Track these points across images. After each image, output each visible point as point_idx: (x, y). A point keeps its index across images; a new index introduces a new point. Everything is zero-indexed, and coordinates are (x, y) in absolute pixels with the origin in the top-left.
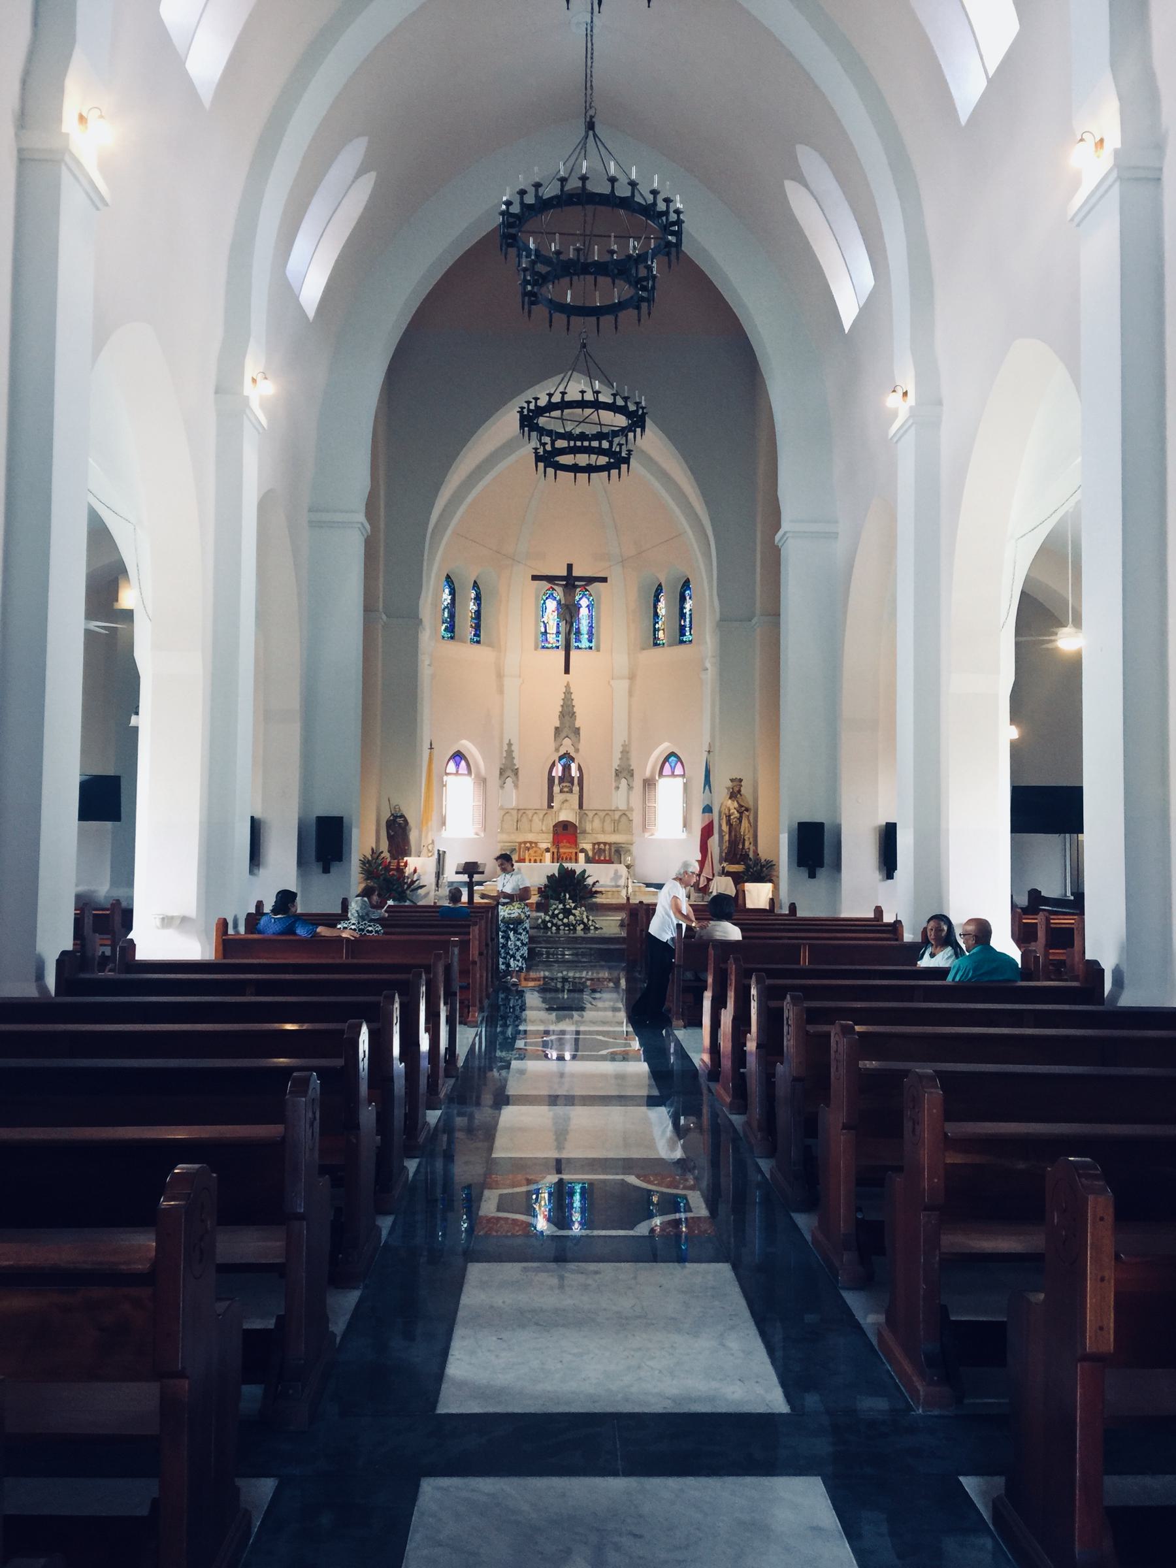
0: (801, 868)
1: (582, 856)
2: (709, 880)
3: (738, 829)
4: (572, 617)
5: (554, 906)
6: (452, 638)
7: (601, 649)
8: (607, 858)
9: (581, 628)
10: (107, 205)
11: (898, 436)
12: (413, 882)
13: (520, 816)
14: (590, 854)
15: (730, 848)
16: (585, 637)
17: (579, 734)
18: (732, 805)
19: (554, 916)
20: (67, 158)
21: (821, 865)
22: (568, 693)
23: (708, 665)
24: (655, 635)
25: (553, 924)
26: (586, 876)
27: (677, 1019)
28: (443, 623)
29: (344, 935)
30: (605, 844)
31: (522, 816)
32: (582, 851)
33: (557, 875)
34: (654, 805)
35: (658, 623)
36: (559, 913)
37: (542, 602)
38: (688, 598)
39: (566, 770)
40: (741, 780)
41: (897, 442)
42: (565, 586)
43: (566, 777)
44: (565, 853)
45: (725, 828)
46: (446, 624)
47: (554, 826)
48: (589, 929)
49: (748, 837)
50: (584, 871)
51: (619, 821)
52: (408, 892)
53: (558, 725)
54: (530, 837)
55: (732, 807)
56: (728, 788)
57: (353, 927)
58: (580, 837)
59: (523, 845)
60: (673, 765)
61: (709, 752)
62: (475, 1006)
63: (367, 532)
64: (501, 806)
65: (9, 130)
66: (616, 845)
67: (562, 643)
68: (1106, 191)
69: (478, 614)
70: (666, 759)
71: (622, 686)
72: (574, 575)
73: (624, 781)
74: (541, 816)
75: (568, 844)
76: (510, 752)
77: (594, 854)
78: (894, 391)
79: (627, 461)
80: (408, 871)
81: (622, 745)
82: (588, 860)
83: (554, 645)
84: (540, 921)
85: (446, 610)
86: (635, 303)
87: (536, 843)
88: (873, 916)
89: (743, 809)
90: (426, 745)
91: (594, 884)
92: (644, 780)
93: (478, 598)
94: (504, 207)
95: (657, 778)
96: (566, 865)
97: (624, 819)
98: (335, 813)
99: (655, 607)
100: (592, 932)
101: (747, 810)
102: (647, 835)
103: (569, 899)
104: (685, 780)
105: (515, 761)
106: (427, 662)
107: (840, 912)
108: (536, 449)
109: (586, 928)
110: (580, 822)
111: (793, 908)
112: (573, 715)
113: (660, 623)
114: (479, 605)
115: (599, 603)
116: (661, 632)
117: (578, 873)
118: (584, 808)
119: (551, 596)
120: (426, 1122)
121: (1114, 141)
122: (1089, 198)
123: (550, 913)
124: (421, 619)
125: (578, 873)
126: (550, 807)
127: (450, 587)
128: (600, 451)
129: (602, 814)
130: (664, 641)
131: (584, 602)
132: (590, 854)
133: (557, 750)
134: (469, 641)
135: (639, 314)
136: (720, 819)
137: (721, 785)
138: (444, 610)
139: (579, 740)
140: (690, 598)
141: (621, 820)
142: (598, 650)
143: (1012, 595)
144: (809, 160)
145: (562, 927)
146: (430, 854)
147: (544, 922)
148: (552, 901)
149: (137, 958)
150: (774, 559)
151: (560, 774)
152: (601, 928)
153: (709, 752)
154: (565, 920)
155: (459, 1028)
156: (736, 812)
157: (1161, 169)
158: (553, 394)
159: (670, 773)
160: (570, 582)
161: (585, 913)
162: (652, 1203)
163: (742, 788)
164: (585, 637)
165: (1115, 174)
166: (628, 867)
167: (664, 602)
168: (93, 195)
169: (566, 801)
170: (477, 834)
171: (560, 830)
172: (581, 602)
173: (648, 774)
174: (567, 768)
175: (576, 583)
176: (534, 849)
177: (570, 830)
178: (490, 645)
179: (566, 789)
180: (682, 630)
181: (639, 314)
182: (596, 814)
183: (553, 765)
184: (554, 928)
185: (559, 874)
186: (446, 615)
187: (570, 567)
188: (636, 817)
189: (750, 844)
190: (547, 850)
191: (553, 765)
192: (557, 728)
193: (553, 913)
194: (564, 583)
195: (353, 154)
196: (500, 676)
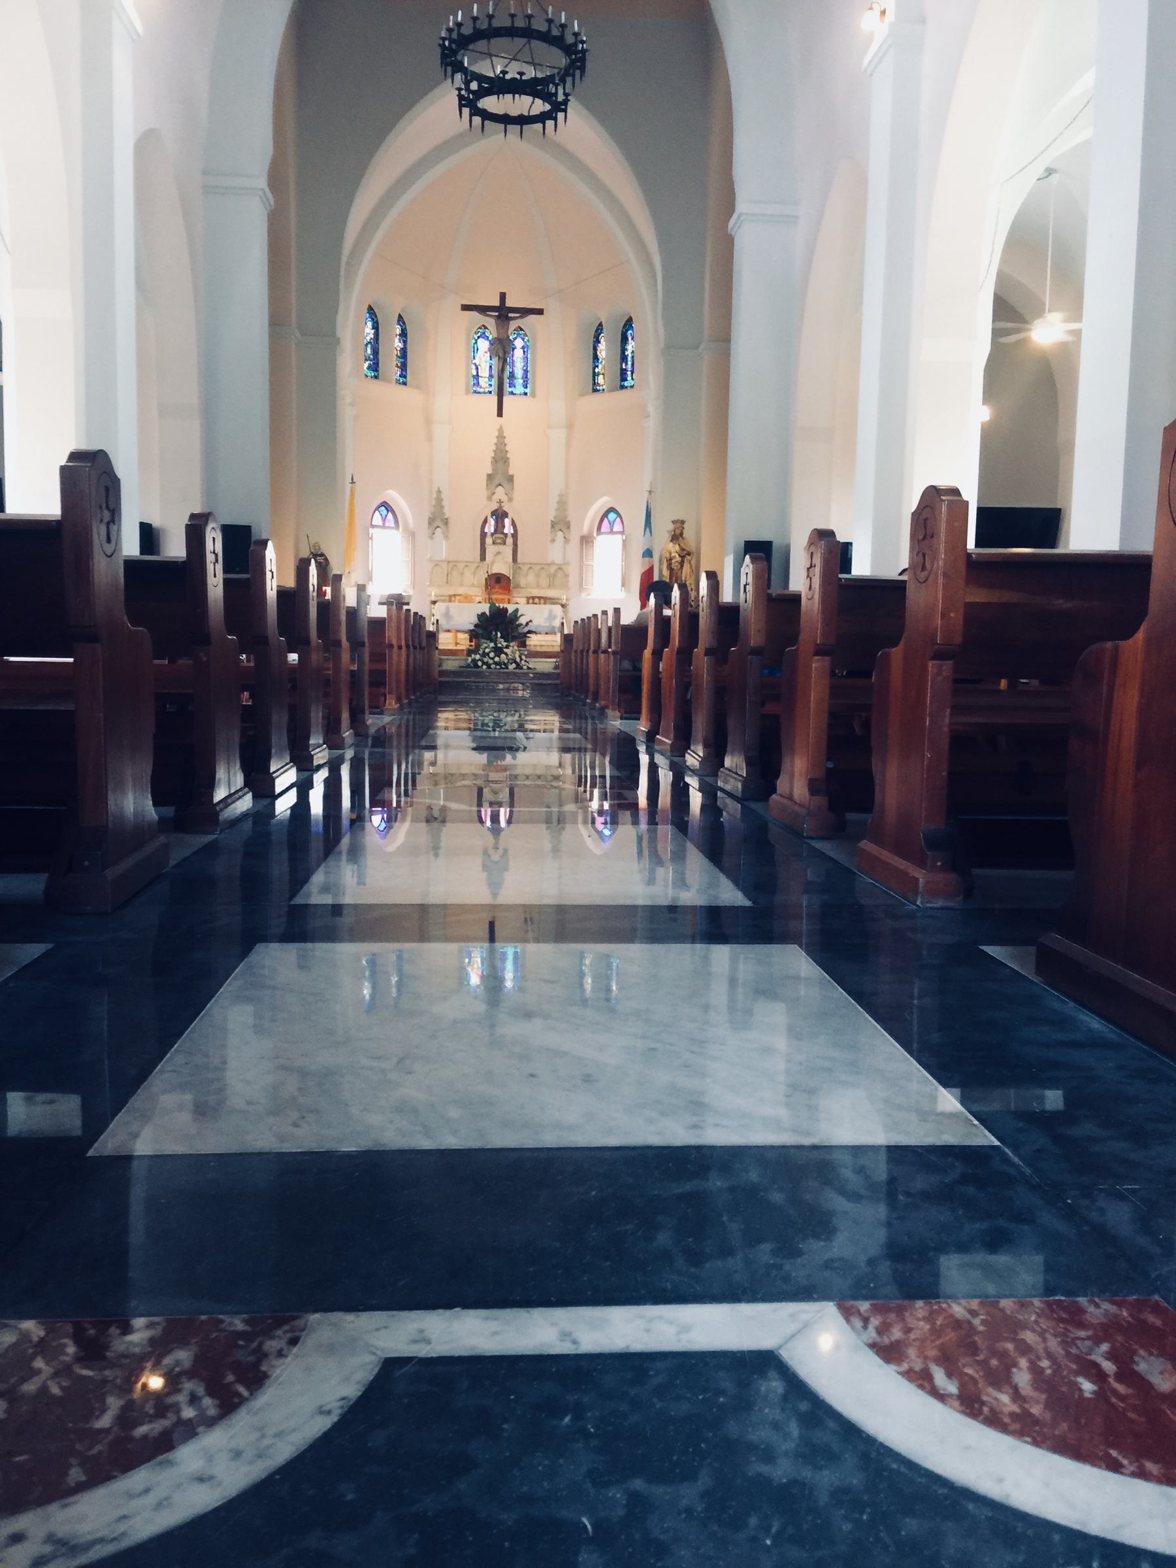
3: (679, 574)
4: (505, 353)
5: (485, 645)
6: (376, 377)
9: (516, 371)
13: (450, 569)
16: (519, 382)
17: (513, 482)
18: (674, 548)
19: (485, 655)
22: (501, 437)
23: (651, 409)
24: (594, 380)
25: (483, 663)
26: (519, 615)
27: (613, 709)
28: (366, 360)
31: (452, 569)
33: (488, 614)
35: (597, 366)
36: (490, 652)
37: (474, 341)
38: (630, 338)
40: (683, 522)
42: (498, 317)
46: (369, 362)
51: (554, 576)
53: (490, 472)
61: (650, 492)
62: (392, 694)
63: (270, 205)
67: (494, 388)
69: (404, 352)
70: (605, 515)
72: (507, 305)
74: (473, 570)
75: (500, 591)
76: (439, 500)
78: (871, 9)
81: (559, 495)
83: (487, 390)
85: (369, 346)
86: (542, 118)
93: (404, 334)
95: (595, 535)
97: (560, 574)
99: (595, 349)
101: (689, 554)
102: (583, 595)
103: (501, 637)
104: (624, 537)
106: (348, 400)
112: (506, 461)
113: (600, 366)
114: (405, 342)
116: (601, 377)
117: (510, 611)
118: (519, 561)
123: (481, 652)
124: (339, 339)
125: (510, 611)
126: (483, 557)
127: (373, 319)
130: (604, 387)
131: (519, 343)
134: (394, 382)
136: (660, 561)
137: (663, 528)
138: (367, 345)
139: (513, 489)
140: (632, 339)
142: (534, 395)
143: (993, 249)
145: (493, 666)
148: (483, 641)
150: (727, 245)
153: (650, 492)
154: (497, 659)
156: (677, 556)
159: (609, 530)
160: (503, 313)
162: (585, 965)
163: (684, 531)
164: (519, 382)
166: (563, 606)
167: (604, 343)
169: (499, 553)
173: (585, 531)
175: (510, 315)
177: (503, 583)
178: (418, 387)
179: (499, 541)
180: (623, 373)
182: (531, 568)
183: (485, 521)
186: (369, 351)
187: (503, 296)
188: (573, 571)
191: (485, 521)
192: (489, 476)
193: (484, 652)
194: (497, 314)
196: (428, 422)
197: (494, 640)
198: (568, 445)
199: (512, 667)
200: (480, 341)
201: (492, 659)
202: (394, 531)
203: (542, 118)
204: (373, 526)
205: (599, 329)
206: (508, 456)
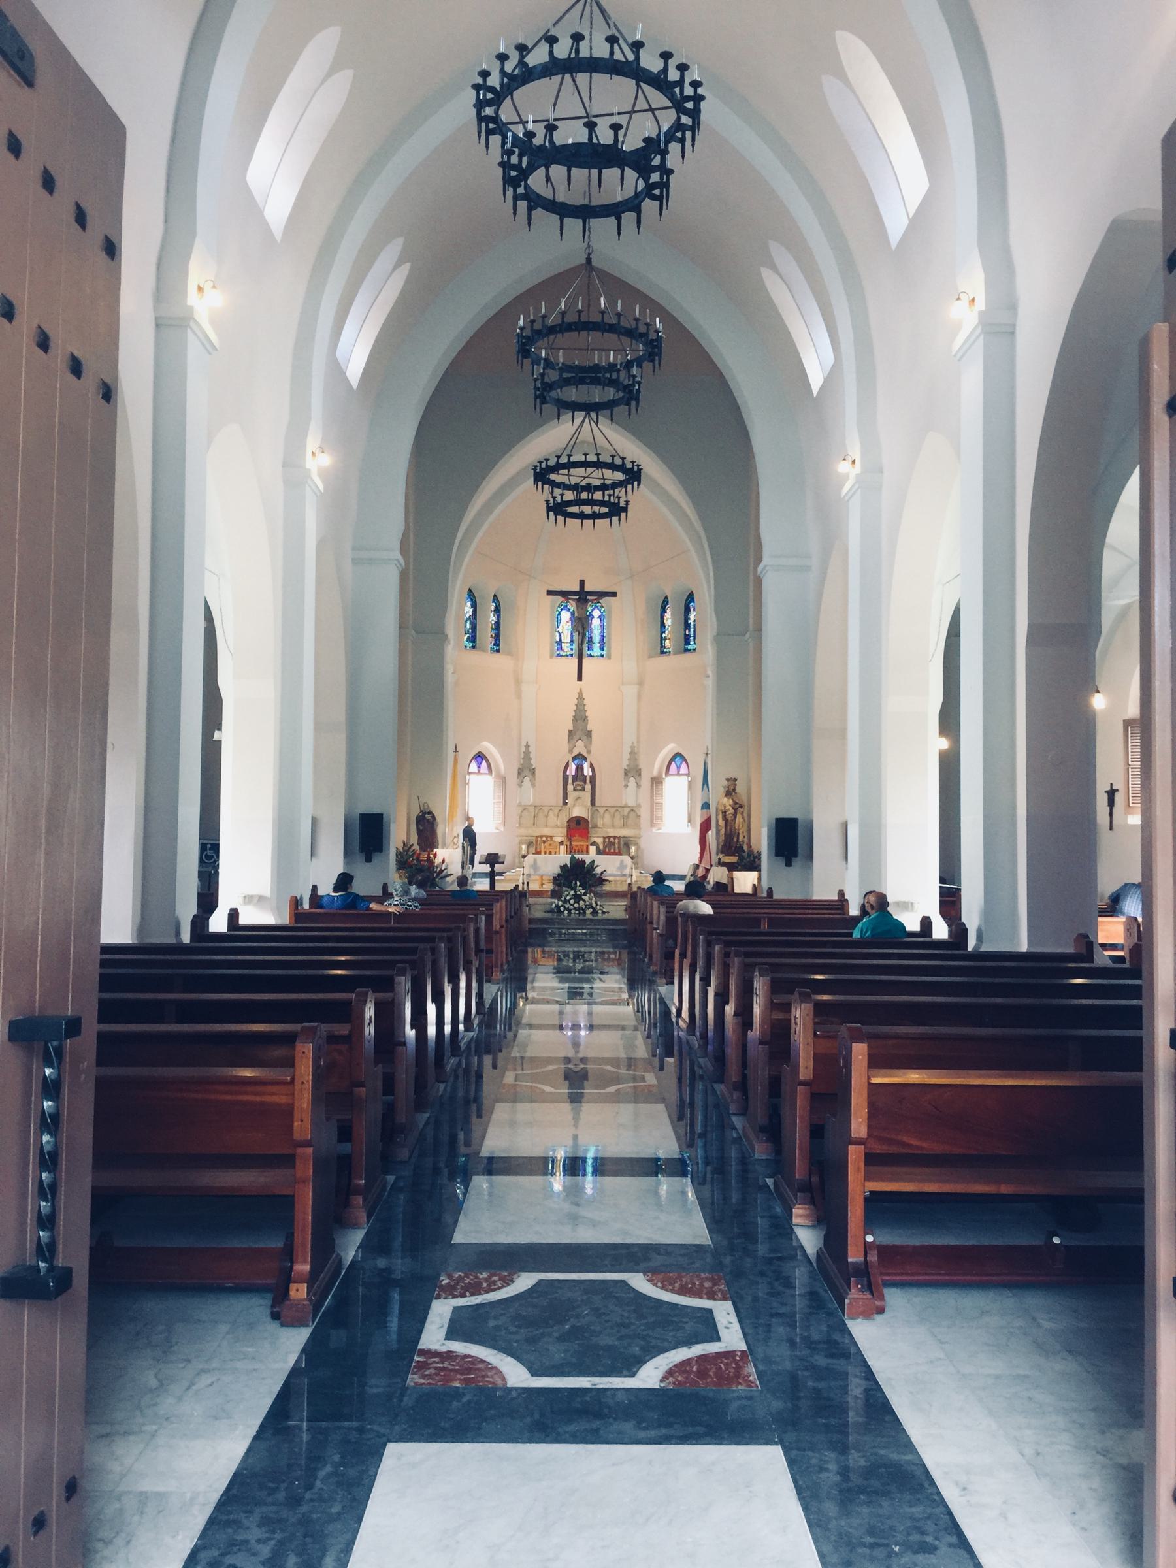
0: (779, 858)
1: (593, 849)
2: (707, 870)
5: (566, 893)
6: (474, 647)
7: (612, 657)
8: (617, 851)
10: (216, 350)
11: (850, 494)
12: (442, 871)
14: (601, 847)
15: (726, 840)
16: (596, 646)
17: (591, 737)
18: (728, 802)
19: (566, 901)
20: (192, 324)
21: (796, 856)
22: (581, 698)
23: (710, 673)
24: (661, 644)
29: (390, 910)
30: (615, 837)
32: (593, 844)
34: (661, 802)
35: (664, 632)
38: (692, 610)
39: (579, 770)
40: (735, 780)
41: (848, 501)
42: (578, 601)
43: (579, 775)
44: (577, 846)
45: (721, 823)
47: (568, 822)
48: (597, 913)
49: (742, 831)
50: (593, 861)
51: (628, 817)
52: (437, 880)
54: (546, 831)
55: (727, 804)
56: (724, 787)
57: (396, 903)
58: (592, 831)
59: (539, 839)
60: (678, 764)
64: (520, 803)
65: (149, 303)
66: (625, 839)
68: (975, 341)
69: (498, 624)
71: (631, 691)
73: (632, 779)
76: (527, 753)
77: (605, 847)
79: (625, 510)
80: (437, 861)
82: (599, 852)
83: (568, 654)
84: (554, 905)
85: (468, 622)
87: (551, 837)
88: (836, 898)
89: (738, 806)
90: (451, 749)
91: (602, 873)
92: (652, 778)
93: (498, 610)
94: (518, 331)
95: (664, 776)
96: (577, 856)
98: (376, 811)
99: (662, 618)
100: (600, 915)
101: (741, 806)
102: (654, 830)
105: (533, 762)
107: (812, 896)
108: (547, 501)
109: (595, 912)
110: (592, 817)
111: (770, 892)
112: (585, 719)
114: (499, 617)
115: (610, 612)
116: (667, 641)
117: (587, 863)
118: (596, 804)
119: (565, 608)
120: (492, 905)
121: (981, 305)
122: (969, 336)
123: (563, 899)
125: (587, 863)
126: (565, 803)
127: (472, 600)
128: (602, 503)
129: (612, 810)
131: (596, 613)
132: (601, 847)
133: (571, 751)
135: (630, 409)
136: (717, 815)
138: (466, 621)
140: (694, 610)
141: (630, 815)
142: (609, 657)
144: (779, 253)
145: (573, 911)
146: (455, 847)
147: (557, 906)
148: (564, 888)
149: (211, 930)
151: (573, 774)
152: (608, 912)
154: (576, 905)
155: (486, 985)
157: (1014, 326)
158: (560, 456)
160: (583, 596)
161: (594, 899)
163: (737, 788)
164: (596, 646)
165: (979, 331)
166: (632, 858)
168: (206, 343)
170: (497, 829)
171: (573, 825)
172: (593, 613)
173: (655, 773)
174: (580, 768)
175: (588, 598)
176: (549, 842)
178: (509, 654)
179: (579, 788)
181: (630, 409)
183: (567, 765)
184: (566, 912)
185: (571, 863)
186: (468, 626)
187: (582, 583)
188: (644, 813)
189: (744, 837)
190: (561, 843)
191: (567, 765)
192: (570, 732)
194: (577, 597)
195: (394, 249)
196: (518, 682)
197: (574, 889)
198: (639, 697)
199: (589, 912)
200: (563, 613)
201: (573, 905)
202: (488, 777)
203: (633, 205)
204: (469, 773)
205: (665, 602)
206: (587, 714)
